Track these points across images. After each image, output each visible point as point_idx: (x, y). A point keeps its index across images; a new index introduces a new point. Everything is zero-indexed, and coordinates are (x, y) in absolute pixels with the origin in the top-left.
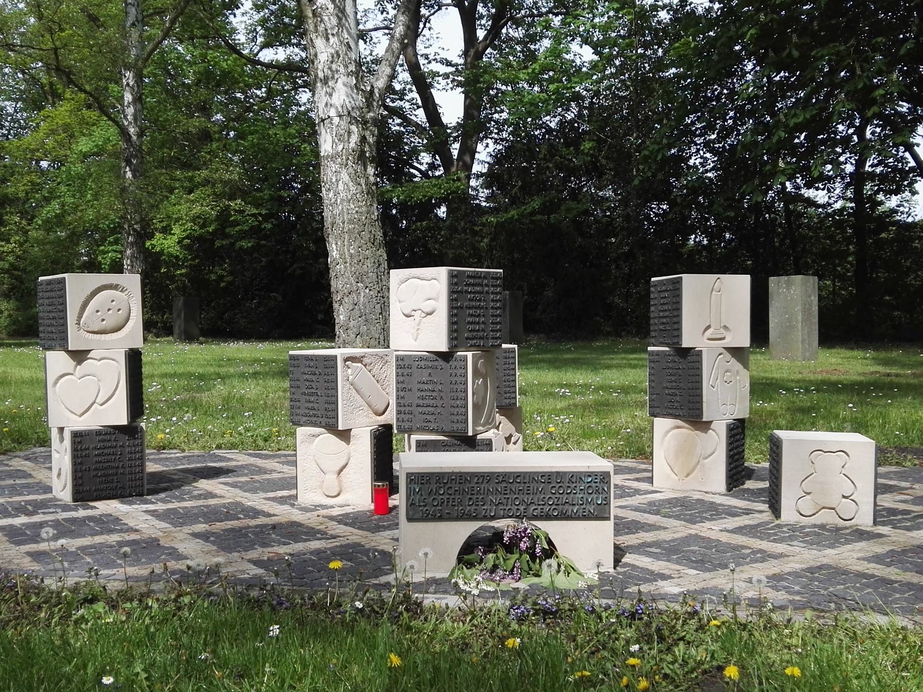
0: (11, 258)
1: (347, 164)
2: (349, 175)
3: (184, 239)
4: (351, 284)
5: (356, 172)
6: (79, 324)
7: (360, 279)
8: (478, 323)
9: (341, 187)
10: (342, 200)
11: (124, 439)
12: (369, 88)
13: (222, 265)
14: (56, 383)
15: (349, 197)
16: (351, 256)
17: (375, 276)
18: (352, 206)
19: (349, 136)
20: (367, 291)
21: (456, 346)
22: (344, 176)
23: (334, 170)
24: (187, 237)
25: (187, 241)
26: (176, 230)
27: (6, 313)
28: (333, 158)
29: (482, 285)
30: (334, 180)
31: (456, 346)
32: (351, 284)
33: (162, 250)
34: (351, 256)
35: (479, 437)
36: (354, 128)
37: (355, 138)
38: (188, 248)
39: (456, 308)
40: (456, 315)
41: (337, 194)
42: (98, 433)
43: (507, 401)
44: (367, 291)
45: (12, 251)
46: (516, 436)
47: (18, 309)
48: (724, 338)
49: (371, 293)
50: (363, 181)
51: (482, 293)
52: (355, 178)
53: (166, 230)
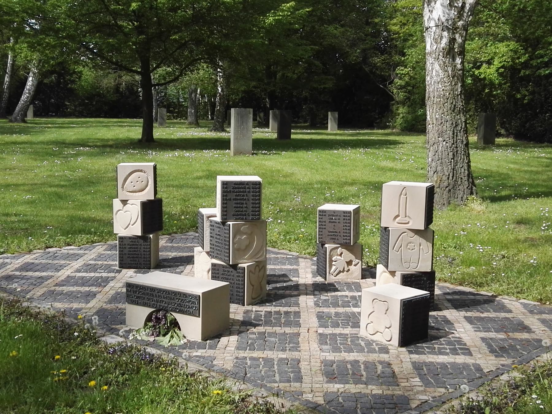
0: (407, 79)
1: (438, 58)
2: (440, 65)
3: (500, 68)
4: (435, 138)
5: (444, 63)
6: (123, 188)
7: (440, 135)
8: (242, 207)
9: (434, 73)
10: (435, 82)
11: (141, 241)
12: (460, 5)
13: (527, 87)
14: (116, 213)
15: (439, 80)
16: (436, 119)
17: (451, 133)
18: (440, 86)
19: (441, 40)
20: (444, 143)
21: (226, 219)
22: (437, 67)
23: (431, 62)
24: (502, 67)
25: (502, 70)
26: (496, 62)
27: (401, 115)
28: (430, 53)
29: (245, 188)
30: (430, 69)
31: (226, 219)
32: (435, 138)
33: (485, 78)
34: (436, 119)
35: (239, 265)
36: (445, 34)
37: (445, 41)
38: (500, 75)
39: (227, 200)
40: (226, 203)
41: (432, 78)
42: (130, 238)
43: (345, 241)
44: (444, 143)
45: (408, 74)
46: (355, 261)
47: (409, 113)
48: (408, 223)
49: (447, 144)
50: (450, 69)
51: (245, 192)
52: (444, 67)
53: (489, 63)
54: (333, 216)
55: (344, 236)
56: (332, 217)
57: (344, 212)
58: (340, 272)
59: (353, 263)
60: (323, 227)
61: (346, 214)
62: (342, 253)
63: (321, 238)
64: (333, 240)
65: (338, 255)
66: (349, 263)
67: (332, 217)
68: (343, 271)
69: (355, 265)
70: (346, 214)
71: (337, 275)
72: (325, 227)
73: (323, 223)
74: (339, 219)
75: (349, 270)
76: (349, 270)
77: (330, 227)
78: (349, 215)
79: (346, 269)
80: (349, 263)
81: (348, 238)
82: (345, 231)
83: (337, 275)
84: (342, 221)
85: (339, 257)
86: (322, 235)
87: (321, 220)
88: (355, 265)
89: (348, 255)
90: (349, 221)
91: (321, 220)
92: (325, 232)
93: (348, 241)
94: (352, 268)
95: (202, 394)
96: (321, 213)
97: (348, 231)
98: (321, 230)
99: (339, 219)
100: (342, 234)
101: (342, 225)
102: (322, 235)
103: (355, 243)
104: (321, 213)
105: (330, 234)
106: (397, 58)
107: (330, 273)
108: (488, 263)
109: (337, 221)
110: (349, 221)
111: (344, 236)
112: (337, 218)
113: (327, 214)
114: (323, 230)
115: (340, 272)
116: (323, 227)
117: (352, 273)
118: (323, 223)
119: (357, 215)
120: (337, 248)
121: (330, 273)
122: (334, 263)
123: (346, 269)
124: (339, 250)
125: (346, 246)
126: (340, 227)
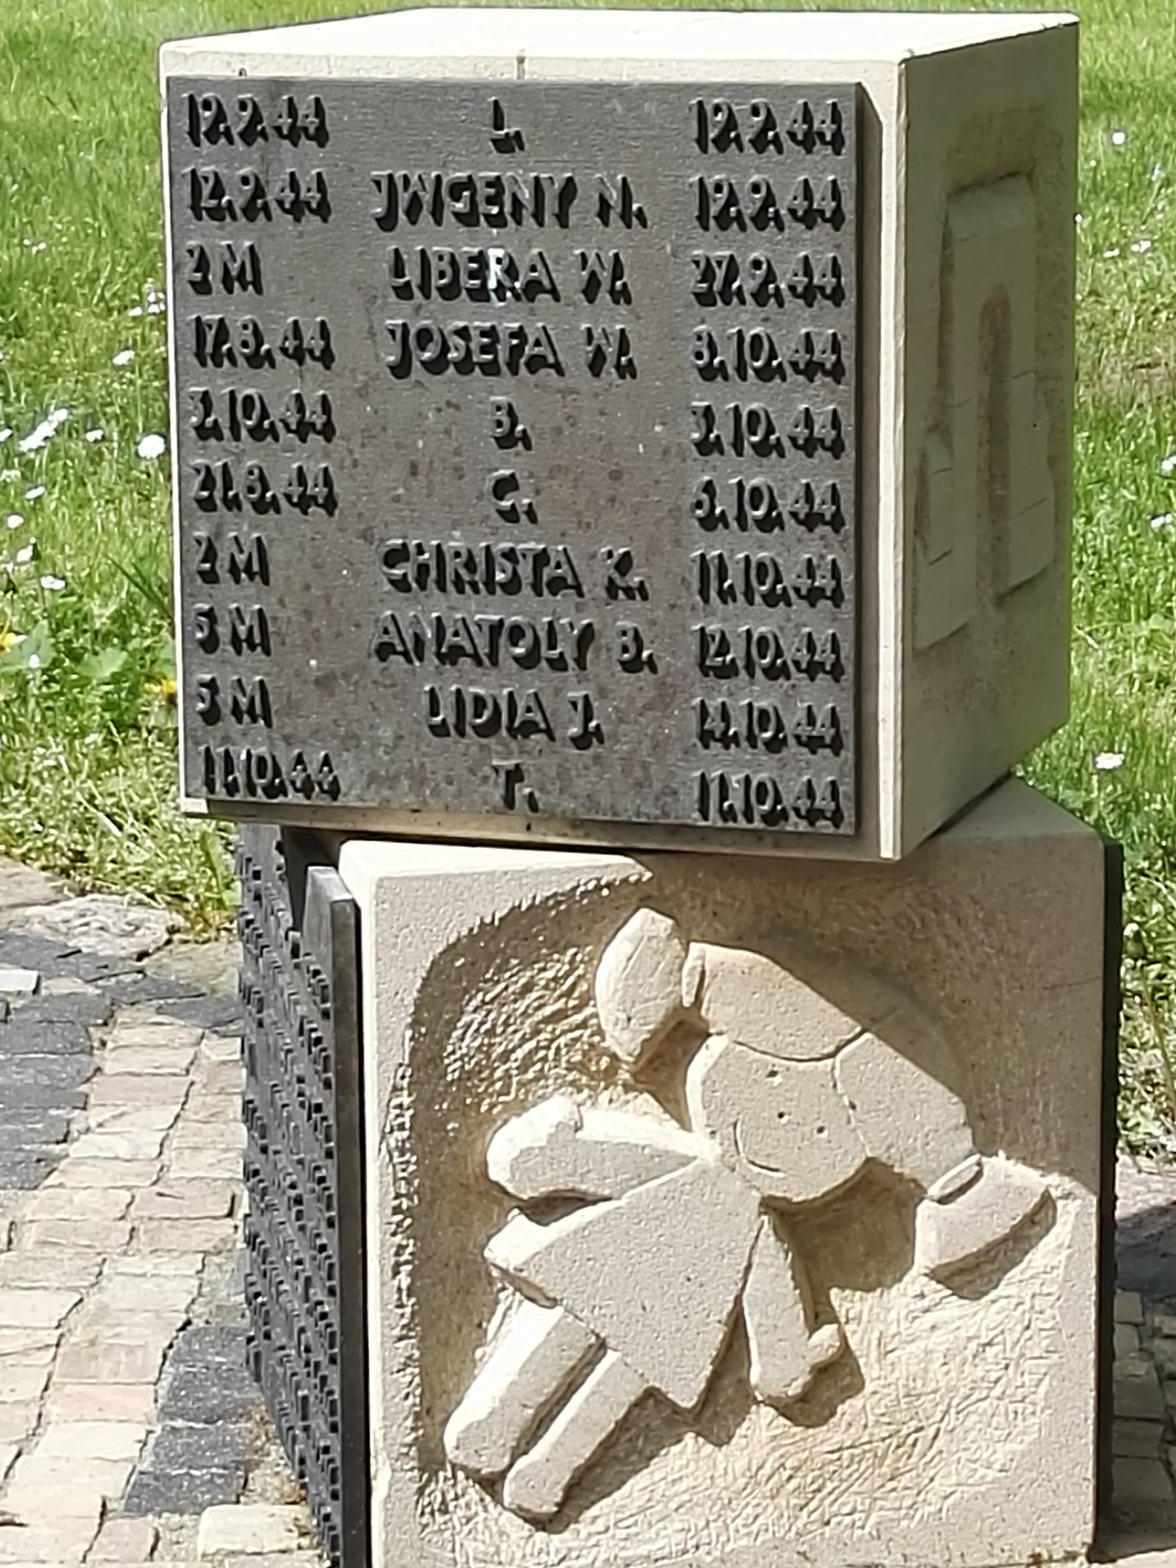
43: (738, 768)
46: (974, 1190)
54: (486, 206)
55: (714, 661)
56: (448, 241)
57: (720, 121)
58: (647, 1426)
59: (933, 1234)
60: (284, 462)
61: (746, 171)
62: (681, 1034)
63: (259, 709)
64: (502, 750)
65: (595, 1072)
66: (842, 1233)
67: (448, 241)
68: (722, 1402)
69: (970, 1276)
70: (746, 171)
71: (585, 1487)
72: (312, 457)
73: (281, 388)
74: (606, 284)
75: (835, 1378)
76: (835, 1378)
77: (414, 461)
78: (827, 170)
79: (777, 1366)
80: (842, 1233)
81: (808, 701)
82: (738, 548)
83: (585, 1487)
84: (667, 325)
85: (626, 1121)
86: (259, 638)
87: (235, 311)
88: (970, 1276)
89: (804, 1076)
90: (828, 324)
91: (235, 311)
92: (326, 573)
93: (800, 775)
94: (899, 1325)
95: (28, 148)
96: (231, 164)
97: (794, 553)
98: (242, 529)
99: (606, 284)
100: (677, 624)
101: (669, 400)
102: (259, 638)
103: (975, 789)
104: (231, 164)
105: (426, 611)
106: (20, 38)
107: (430, 1459)
108: (1157, 1119)
109: (568, 324)
110: (828, 324)
111: (714, 661)
112: (566, 250)
113: (353, 171)
114: (287, 534)
115: (647, 1426)
116: (284, 462)
117: (908, 1440)
118: (281, 388)
119: (1011, 212)
120: (567, 924)
121: (430, 1459)
122: (515, 1243)
123: (777, 1366)
124: (630, 970)
125: (768, 871)
126: (626, 460)
